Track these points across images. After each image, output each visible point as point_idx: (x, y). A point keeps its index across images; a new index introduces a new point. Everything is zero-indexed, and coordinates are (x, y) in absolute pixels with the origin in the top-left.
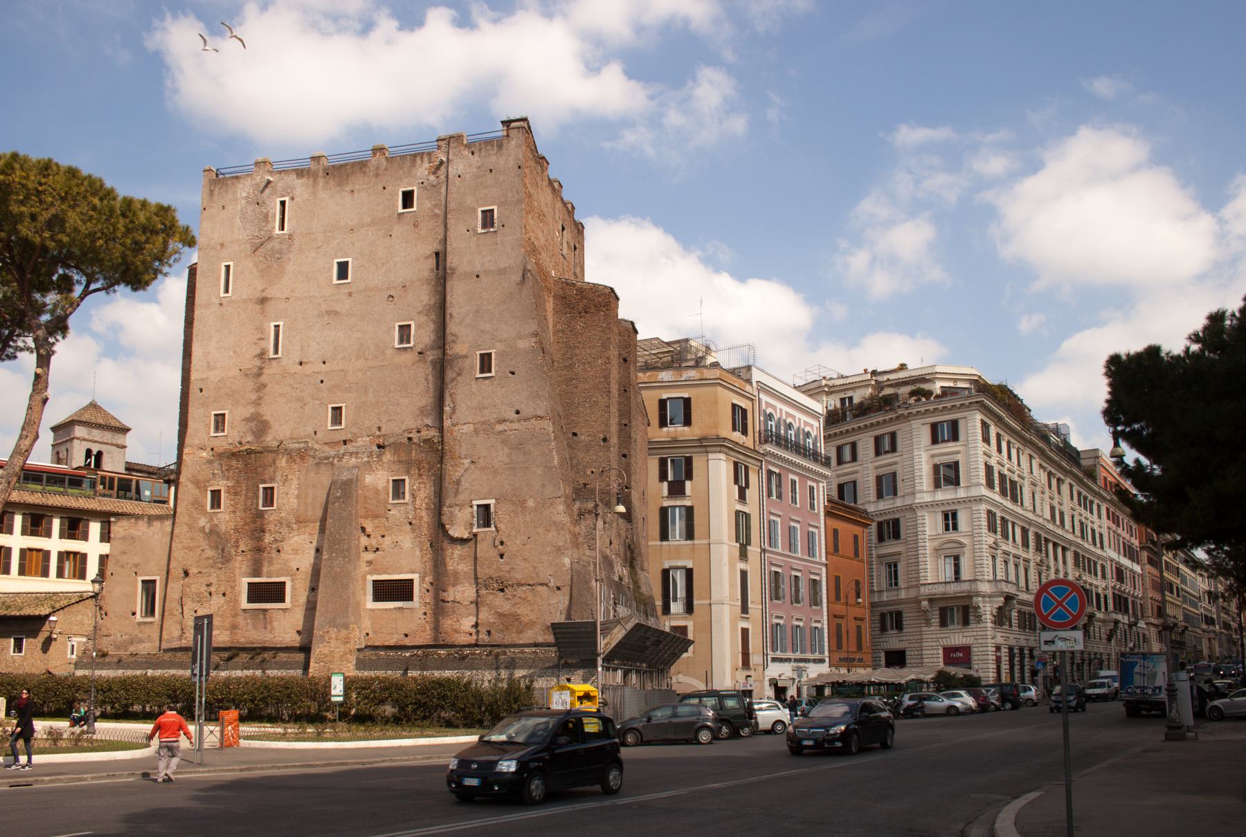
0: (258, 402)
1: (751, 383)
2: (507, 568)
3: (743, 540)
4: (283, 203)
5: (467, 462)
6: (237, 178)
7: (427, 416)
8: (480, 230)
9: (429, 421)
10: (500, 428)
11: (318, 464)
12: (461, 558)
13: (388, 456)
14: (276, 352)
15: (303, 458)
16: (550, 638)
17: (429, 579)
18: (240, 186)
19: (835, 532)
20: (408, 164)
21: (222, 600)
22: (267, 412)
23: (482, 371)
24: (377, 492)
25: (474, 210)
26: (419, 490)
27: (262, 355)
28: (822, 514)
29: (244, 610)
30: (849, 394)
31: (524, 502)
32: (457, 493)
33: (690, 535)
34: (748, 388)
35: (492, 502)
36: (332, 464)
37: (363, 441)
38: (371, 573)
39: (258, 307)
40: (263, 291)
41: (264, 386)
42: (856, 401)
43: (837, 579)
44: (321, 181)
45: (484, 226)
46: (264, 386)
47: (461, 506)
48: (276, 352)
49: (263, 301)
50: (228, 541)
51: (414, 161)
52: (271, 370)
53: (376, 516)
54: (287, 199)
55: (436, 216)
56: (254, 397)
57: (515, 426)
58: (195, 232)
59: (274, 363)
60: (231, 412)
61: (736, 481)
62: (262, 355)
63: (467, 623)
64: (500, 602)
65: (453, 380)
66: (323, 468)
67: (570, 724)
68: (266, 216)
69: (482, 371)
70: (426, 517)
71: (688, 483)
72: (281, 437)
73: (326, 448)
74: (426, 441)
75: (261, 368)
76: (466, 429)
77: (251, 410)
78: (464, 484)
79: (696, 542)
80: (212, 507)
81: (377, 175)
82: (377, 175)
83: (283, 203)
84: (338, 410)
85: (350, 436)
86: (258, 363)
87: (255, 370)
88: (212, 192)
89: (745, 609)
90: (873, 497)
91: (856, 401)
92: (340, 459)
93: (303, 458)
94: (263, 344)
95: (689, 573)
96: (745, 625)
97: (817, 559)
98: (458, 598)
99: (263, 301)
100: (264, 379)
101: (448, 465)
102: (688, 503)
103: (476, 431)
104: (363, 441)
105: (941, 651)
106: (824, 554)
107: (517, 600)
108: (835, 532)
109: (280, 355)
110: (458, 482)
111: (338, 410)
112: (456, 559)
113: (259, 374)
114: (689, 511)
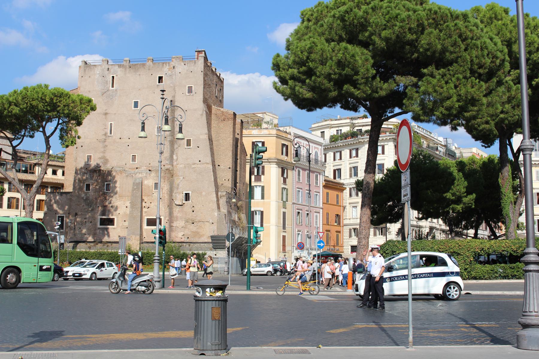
0: (104, 152)
1: (290, 134)
2: (195, 215)
3: (285, 200)
4: (113, 77)
5: (181, 178)
6: (95, 65)
7: (168, 160)
8: (187, 94)
9: (168, 162)
10: (193, 166)
11: (127, 176)
12: (179, 211)
13: (153, 174)
14: (111, 133)
15: (121, 173)
16: (210, 241)
17: (167, 218)
18: (96, 69)
19: (327, 194)
20: (161, 66)
21: (90, 224)
22: (108, 156)
23: (187, 146)
24: (149, 187)
25: (185, 86)
26: (165, 187)
27: (105, 134)
28: (321, 186)
29: (99, 228)
30: (340, 128)
31: (202, 193)
32: (178, 189)
33: (263, 197)
34: (289, 136)
35: (190, 192)
36: (132, 176)
37: (144, 168)
38: (146, 216)
39: (104, 116)
40: (106, 110)
41: (106, 146)
42: (343, 132)
43: (328, 214)
44: (128, 70)
45: (188, 93)
46: (106, 146)
47: (179, 193)
48: (111, 133)
49: (106, 114)
50: (93, 203)
51: (163, 65)
52: (109, 140)
53: (149, 196)
54: (114, 75)
55: (171, 87)
56: (102, 150)
57: (199, 166)
58: (94, 102)
59: (110, 138)
60: (94, 155)
61: (283, 175)
62: (105, 134)
63: (180, 235)
64: (193, 228)
65: (177, 148)
66: (129, 177)
67: (501, 118)
68: (107, 81)
69: (187, 146)
70: (166, 197)
71: (262, 176)
72: (113, 166)
73: (130, 170)
74: (167, 169)
75: (105, 139)
76: (181, 166)
77: (102, 155)
78: (180, 186)
79: (265, 200)
80: (86, 190)
81: (149, 69)
82: (149, 69)
83: (113, 77)
84: (134, 157)
85: (138, 166)
86: (104, 137)
87: (103, 140)
88: (85, 70)
89: (284, 227)
90: (348, 177)
91: (343, 132)
92: (135, 174)
93: (121, 173)
94: (106, 130)
95: (262, 213)
96: (284, 234)
97: (318, 206)
98: (177, 226)
99: (106, 114)
100: (106, 143)
101: (175, 178)
102: (262, 185)
103: (185, 167)
104: (144, 168)
105: (350, 247)
106: (321, 204)
107: (198, 227)
108: (327, 194)
109: (112, 135)
110: (178, 185)
111: (134, 157)
112: (177, 211)
113: (105, 141)
114: (263, 188)
